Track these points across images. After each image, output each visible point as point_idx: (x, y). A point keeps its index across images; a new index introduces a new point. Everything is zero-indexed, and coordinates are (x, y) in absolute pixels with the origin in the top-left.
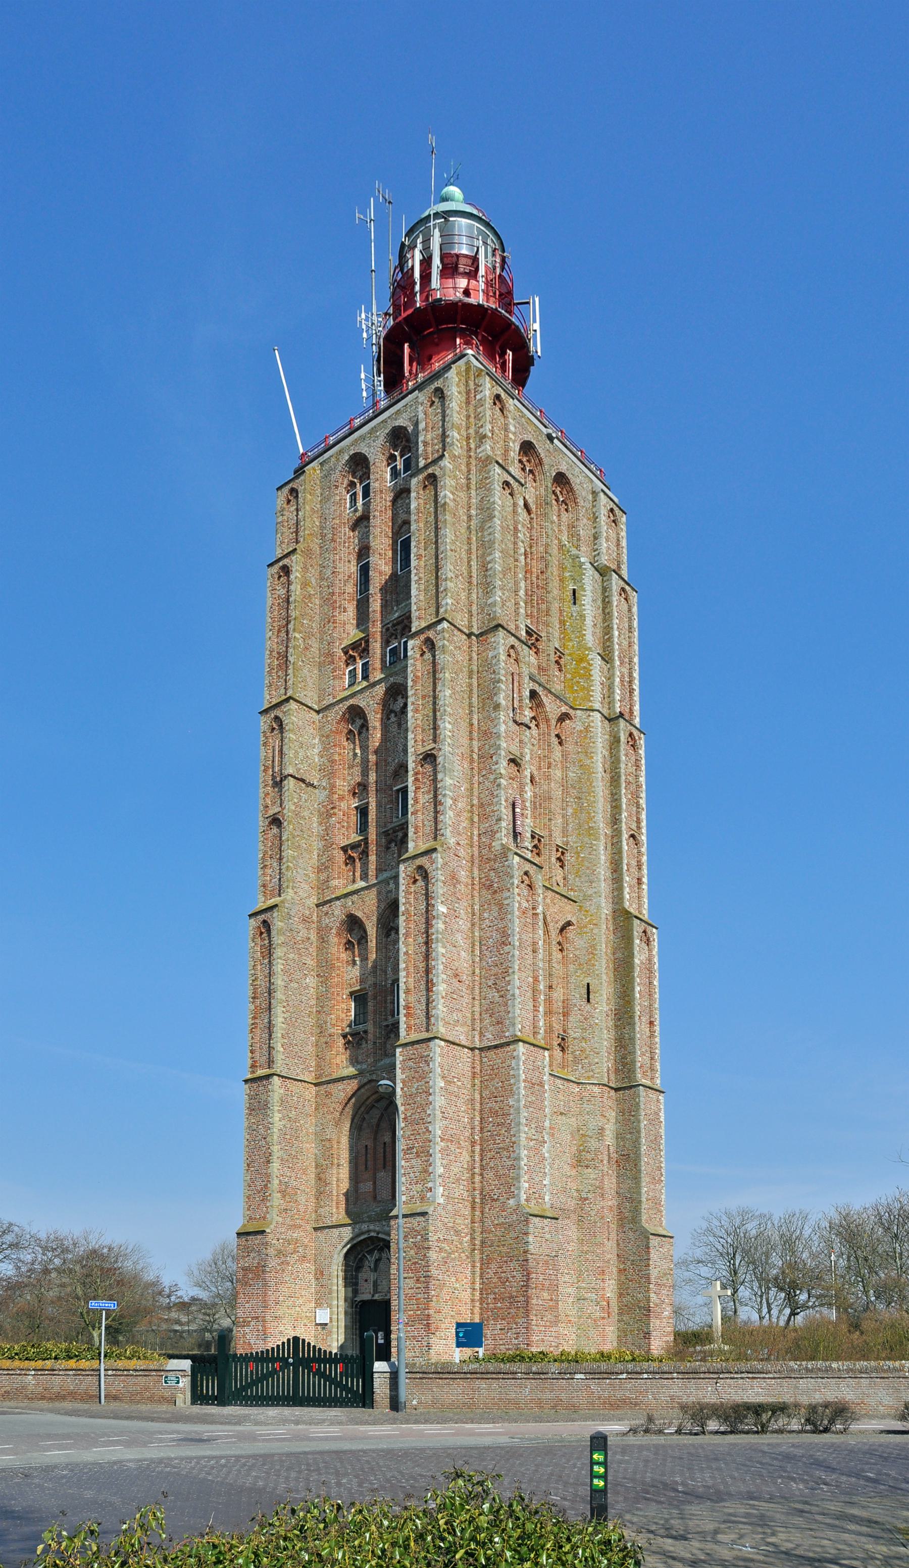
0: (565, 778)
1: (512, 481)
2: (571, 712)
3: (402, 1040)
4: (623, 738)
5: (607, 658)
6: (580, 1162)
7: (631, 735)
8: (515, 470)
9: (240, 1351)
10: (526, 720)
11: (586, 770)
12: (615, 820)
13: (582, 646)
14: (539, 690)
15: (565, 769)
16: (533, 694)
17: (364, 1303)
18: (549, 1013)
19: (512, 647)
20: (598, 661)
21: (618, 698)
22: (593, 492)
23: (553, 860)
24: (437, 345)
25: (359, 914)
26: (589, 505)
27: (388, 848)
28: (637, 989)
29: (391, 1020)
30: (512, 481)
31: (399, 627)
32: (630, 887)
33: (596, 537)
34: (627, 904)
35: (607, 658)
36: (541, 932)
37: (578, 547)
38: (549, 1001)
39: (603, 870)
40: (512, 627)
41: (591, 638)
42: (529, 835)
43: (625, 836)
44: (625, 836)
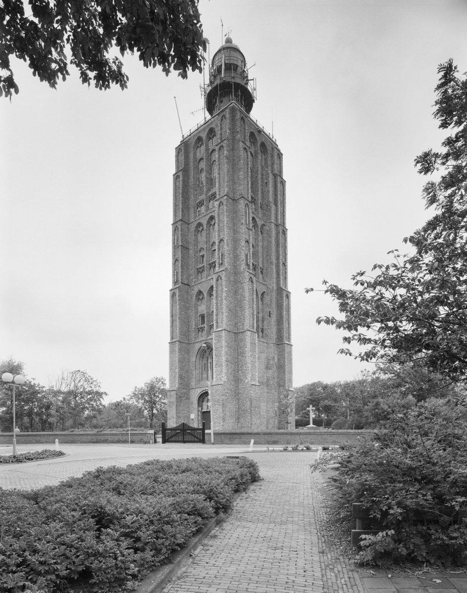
0: (263, 245)
1: (247, 147)
2: (265, 223)
3: (215, 330)
4: (281, 231)
5: (276, 205)
6: (267, 368)
7: (283, 230)
8: (248, 144)
9: (168, 427)
10: (251, 228)
11: (270, 242)
12: (278, 259)
13: (268, 201)
14: (255, 217)
15: (263, 242)
16: (253, 218)
17: (204, 412)
18: (257, 321)
19: (247, 204)
20: (274, 206)
21: (279, 218)
22: (272, 148)
23: (259, 272)
24: (224, 97)
25: (202, 290)
26: (271, 152)
27: (210, 269)
28: (284, 313)
29: (212, 323)
30: (247, 147)
31: (213, 196)
32: (283, 280)
33: (273, 164)
34: (281, 286)
35: (276, 205)
36: (255, 296)
37: (267, 167)
38: (257, 317)
39: (274, 275)
40: (246, 197)
41: (271, 199)
42: (251, 265)
43: (281, 264)
44: (281, 264)
